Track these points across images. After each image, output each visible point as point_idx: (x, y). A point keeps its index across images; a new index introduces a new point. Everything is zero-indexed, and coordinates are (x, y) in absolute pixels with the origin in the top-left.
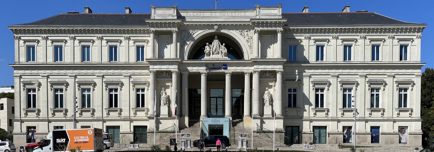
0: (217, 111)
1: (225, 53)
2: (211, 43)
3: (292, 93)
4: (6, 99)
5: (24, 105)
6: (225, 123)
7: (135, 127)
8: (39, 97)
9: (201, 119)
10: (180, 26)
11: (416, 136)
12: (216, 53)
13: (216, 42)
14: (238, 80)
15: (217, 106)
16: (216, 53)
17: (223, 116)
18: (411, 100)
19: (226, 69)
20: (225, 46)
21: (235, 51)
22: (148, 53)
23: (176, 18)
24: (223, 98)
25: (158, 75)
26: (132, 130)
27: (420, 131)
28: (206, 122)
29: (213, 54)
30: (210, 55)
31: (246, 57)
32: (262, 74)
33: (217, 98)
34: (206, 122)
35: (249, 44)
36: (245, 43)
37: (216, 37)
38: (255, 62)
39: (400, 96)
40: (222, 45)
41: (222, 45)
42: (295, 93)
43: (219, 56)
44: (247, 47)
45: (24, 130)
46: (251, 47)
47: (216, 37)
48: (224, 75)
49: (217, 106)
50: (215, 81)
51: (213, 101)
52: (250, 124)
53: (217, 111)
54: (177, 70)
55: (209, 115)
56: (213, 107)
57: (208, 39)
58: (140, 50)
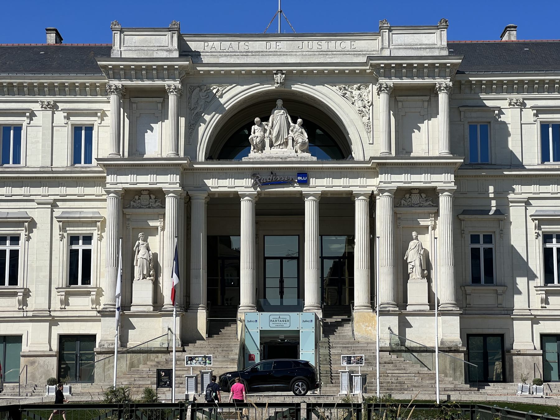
0: (282, 293)
3: (482, 246)
6: (303, 323)
7: (63, 338)
9: (241, 315)
10: (185, 76)
12: (280, 142)
13: (279, 117)
14: (337, 212)
15: (282, 282)
16: (280, 142)
17: (299, 307)
19: (305, 183)
20: (303, 126)
21: (328, 137)
22: (104, 145)
25: (128, 200)
26: (55, 346)
28: (252, 324)
29: (271, 145)
30: (263, 148)
31: (357, 153)
32: (401, 197)
33: (281, 259)
34: (252, 324)
35: (365, 119)
36: (355, 117)
37: (279, 103)
38: (380, 167)
40: (295, 122)
41: (295, 122)
42: (488, 246)
43: (288, 152)
46: (369, 127)
47: (279, 103)
48: (300, 199)
49: (282, 282)
50: (279, 215)
51: (272, 267)
53: (282, 293)
55: (261, 304)
56: (272, 283)
58: (82, 138)
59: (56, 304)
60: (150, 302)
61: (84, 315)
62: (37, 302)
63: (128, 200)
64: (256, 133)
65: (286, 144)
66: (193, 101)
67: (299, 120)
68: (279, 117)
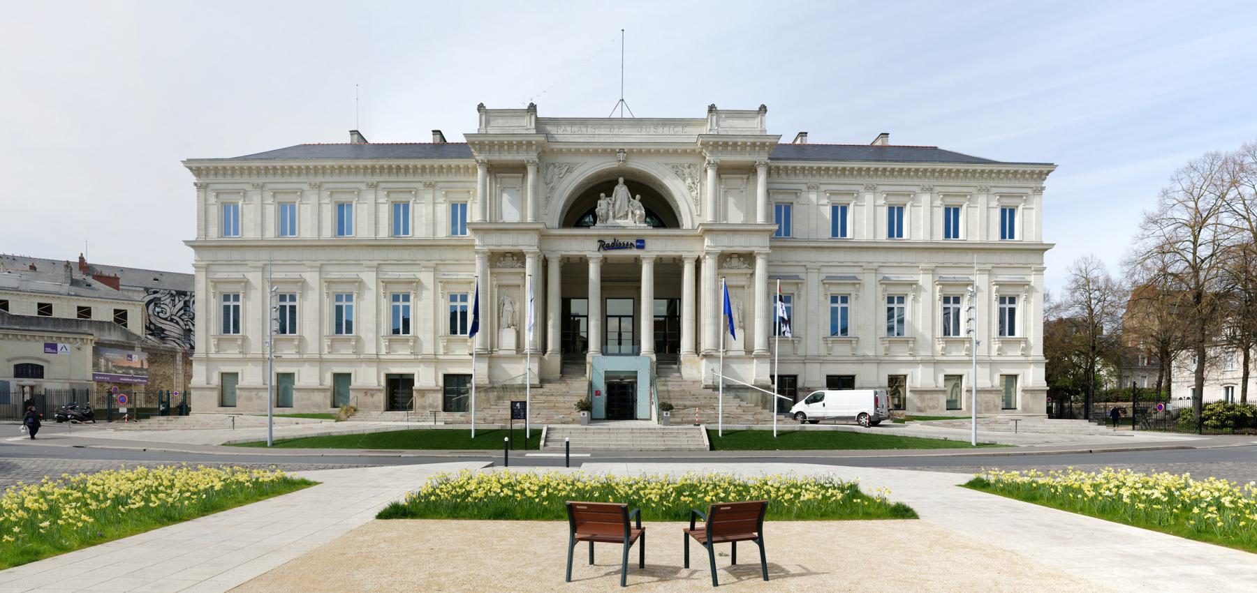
0: (620, 344)
1: (641, 216)
2: (609, 195)
4: (765, 524)
5: (216, 325)
6: (642, 362)
7: (446, 377)
8: (245, 312)
9: (589, 358)
10: (542, 154)
11: (920, 411)
12: (623, 215)
13: (621, 191)
14: (669, 275)
15: (620, 335)
16: (623, 215)
17: (636, 352)
18: (1025, 320)
19: (642, 247)
21: (661, 212)
22: (474, 214)
23: (534, 132)
24: (635, 318)
25: (496, 259)
26: (441, 383)
27: (1043, 385)
28: (600, 365)
29: (614, 217)
30: (607, 219)
31: (686, 222)
32: (724, 258)
33: (620, 317)
34: (600, 365)
35: (694, 194)
36: (686, 192)
37: (621, 180)
38: (708, 231)
39: (1002, 311)
43: (629, 222)
44: (690, 200)
45: (216, 380)
46: (698, 202)
47: (621, 180)
48: (637, 263)
49: (620, 335)
50: (621, 280)
51: (613, 324)
52: (695, 370)
53: (620, 344)
54: (535, 249)
55: (604, 351)
56: (613, 336)
57: (603, 185)
58: (458, 211)
59: (994, 352)
60: (513, 346)
61: (464, 357)
62: (370, 349)
63: (496, 259)
64: (602, 205)
65: (626, 216)
66: (549, 177)
67: (638, 197)
68: (621, 191)
